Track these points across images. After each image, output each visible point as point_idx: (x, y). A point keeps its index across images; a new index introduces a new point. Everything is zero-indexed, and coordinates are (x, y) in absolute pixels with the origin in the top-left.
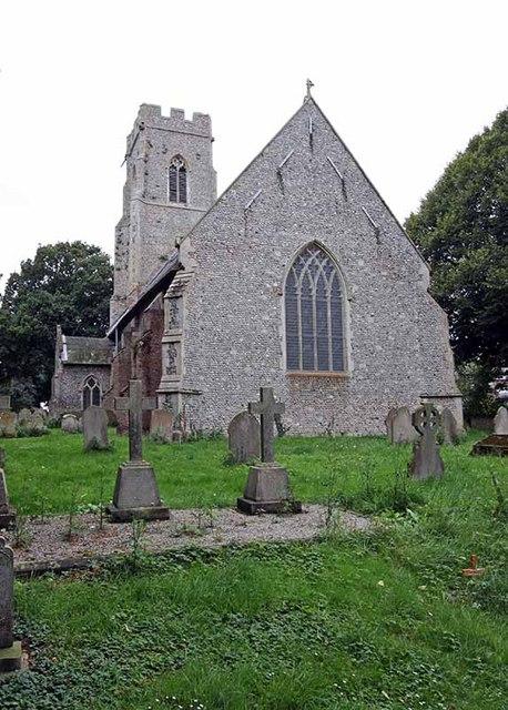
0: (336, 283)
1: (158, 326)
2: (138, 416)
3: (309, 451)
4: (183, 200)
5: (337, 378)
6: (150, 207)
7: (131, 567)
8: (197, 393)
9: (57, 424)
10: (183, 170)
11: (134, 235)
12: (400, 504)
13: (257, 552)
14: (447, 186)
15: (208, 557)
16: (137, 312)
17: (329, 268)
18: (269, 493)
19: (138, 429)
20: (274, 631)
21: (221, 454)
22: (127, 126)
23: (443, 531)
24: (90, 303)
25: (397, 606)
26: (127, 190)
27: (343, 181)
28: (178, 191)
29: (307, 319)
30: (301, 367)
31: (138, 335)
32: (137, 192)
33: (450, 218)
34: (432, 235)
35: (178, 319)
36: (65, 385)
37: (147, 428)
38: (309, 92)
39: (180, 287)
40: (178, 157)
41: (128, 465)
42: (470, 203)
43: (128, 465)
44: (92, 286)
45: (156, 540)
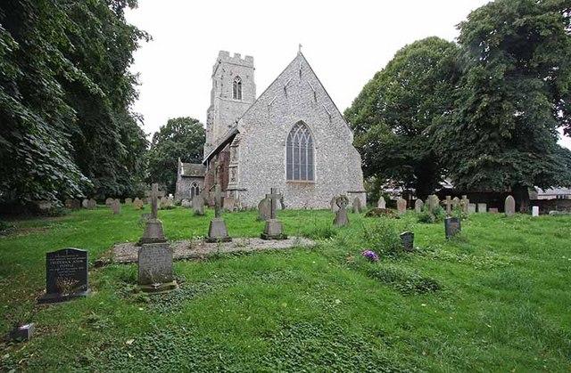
0: (310, 141)
1: (227, 159)
2: (219, 200)
3: (295, 216)
4: (240, 98)
7: (217, 257)
8: (245, 190)
9: (179, 204)
10: (239, 83)
11: (216, 115)
12: (327, 235)
13: (267, 252)
14: (364, 95)
15: (247, 254)
16: (217, 152)
17: (307, 133)
18: (273, 231)
19: (218, 206)
20: (271, 276)
21: (255, 217)
22: (214, 62)
23: (342, 244)
24: (194, 146)
25: (319, 269)
26: (213, 93)
28: (237, 93)
29: (297, 157)
31: (218, 163)
32: (217, 94)
33: (365, 110)
34: (357, 117)
36: (182, 186)
37: (222, 206)
39: (237, 142)
40: (237, 77)
41: (215, 220)
42: (375, 103)
43: (215, 220)
44: (194, 139)
45: (226, 248)
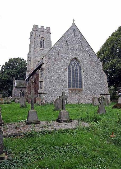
0: (80, 67)
1: (38, 78)
2: (33, 99)
3: (74, 107)
4: (44, 48)
5: (80, 90)
6: (36, 49)
7: (31, 135)
8: (47, 94)
9: (14, 101)
10: (44, 40)
11: (32, 56)
12: (95, 120)
13: (61, 131)
14: (106, 44)
15: (49, 133)
16: (33, 74)
17: (78, 64)
18: (64, 117)
19: (33, 102)
20: (65, 150)
21: (53, 108)
22: (30, 30)
23: (106, 126)
24: (21, 72)
25: (95, 144)
26: (30, 45)
27: (82, 43)
28: (42, 45)
29: (73, 76)
30: (72, 87)
31: (33, 80)
32: (33, 46)
33: (107, 52)
34: (103, 56)
35: (42, 76)
36: (16, 92)
37: (35, 102)
38: (74, 22)
39: (43, 68)
40: (42, 37)
41: (30, 111)
42: (112, 48)
43: (30, 111)
44: (22, 68)
45: (37, 128)
